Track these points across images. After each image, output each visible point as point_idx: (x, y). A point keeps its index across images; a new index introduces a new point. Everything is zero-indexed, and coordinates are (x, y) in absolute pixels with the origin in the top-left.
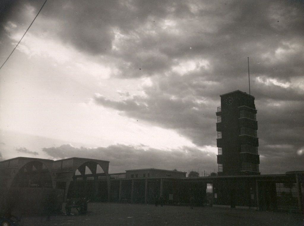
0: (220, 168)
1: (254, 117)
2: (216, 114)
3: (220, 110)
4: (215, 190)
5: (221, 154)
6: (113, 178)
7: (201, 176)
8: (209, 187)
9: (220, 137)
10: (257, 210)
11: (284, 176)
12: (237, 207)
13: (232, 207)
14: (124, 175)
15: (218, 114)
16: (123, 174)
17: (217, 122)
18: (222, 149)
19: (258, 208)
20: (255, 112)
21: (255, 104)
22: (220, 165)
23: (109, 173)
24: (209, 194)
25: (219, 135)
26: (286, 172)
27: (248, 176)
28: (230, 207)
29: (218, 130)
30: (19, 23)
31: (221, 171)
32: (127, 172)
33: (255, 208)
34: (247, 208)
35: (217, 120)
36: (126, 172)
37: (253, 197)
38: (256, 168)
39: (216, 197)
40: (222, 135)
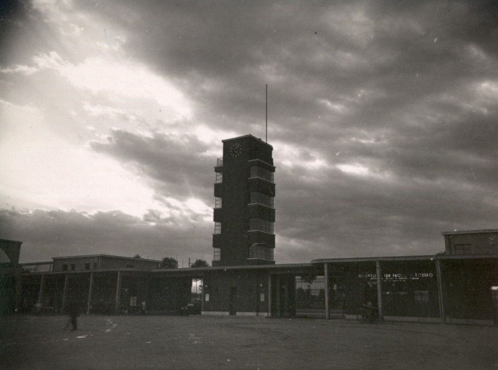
0: (217, 254)
1: (270, 177)
2: (214, 169)
3: (221, 164)
4: (205, 289)
5: (218, 232)
6: (28, 271)
7: (182, 267)
8: (197, 285)
9: (220, 181)
10: (268, 317)
11: (389, 282)
12: (238, 314)
13: (230, 314)
14: (48, 266)
15: (217, 170)
16: (46, 263)
17: (214, 233)
18: (220, 224)
19: (270, 314)
20: (273, 169)
21: (273, 157)
22: (218, 224)
23: (20, 262)
24: (196, 295)
25: (217, 202)
26: (312, 261)
27: (277, 273)
28: (227, 313)
29: (215, 245)
30: (201, 233)
31: (218, 259)
32: (54, 260)
33: (266, 314)
34: (253, 314)
35: (213, 256)
36: (53, 260)
37: (262, 299)
38: (270, 254)
39: (207, 299)
40: (224, 179)
